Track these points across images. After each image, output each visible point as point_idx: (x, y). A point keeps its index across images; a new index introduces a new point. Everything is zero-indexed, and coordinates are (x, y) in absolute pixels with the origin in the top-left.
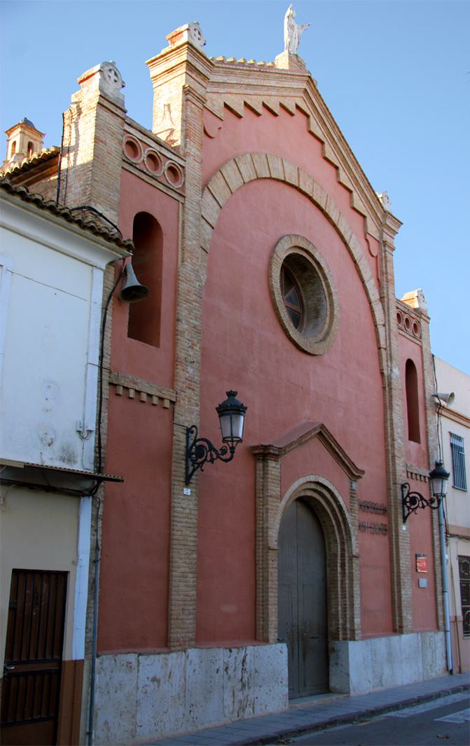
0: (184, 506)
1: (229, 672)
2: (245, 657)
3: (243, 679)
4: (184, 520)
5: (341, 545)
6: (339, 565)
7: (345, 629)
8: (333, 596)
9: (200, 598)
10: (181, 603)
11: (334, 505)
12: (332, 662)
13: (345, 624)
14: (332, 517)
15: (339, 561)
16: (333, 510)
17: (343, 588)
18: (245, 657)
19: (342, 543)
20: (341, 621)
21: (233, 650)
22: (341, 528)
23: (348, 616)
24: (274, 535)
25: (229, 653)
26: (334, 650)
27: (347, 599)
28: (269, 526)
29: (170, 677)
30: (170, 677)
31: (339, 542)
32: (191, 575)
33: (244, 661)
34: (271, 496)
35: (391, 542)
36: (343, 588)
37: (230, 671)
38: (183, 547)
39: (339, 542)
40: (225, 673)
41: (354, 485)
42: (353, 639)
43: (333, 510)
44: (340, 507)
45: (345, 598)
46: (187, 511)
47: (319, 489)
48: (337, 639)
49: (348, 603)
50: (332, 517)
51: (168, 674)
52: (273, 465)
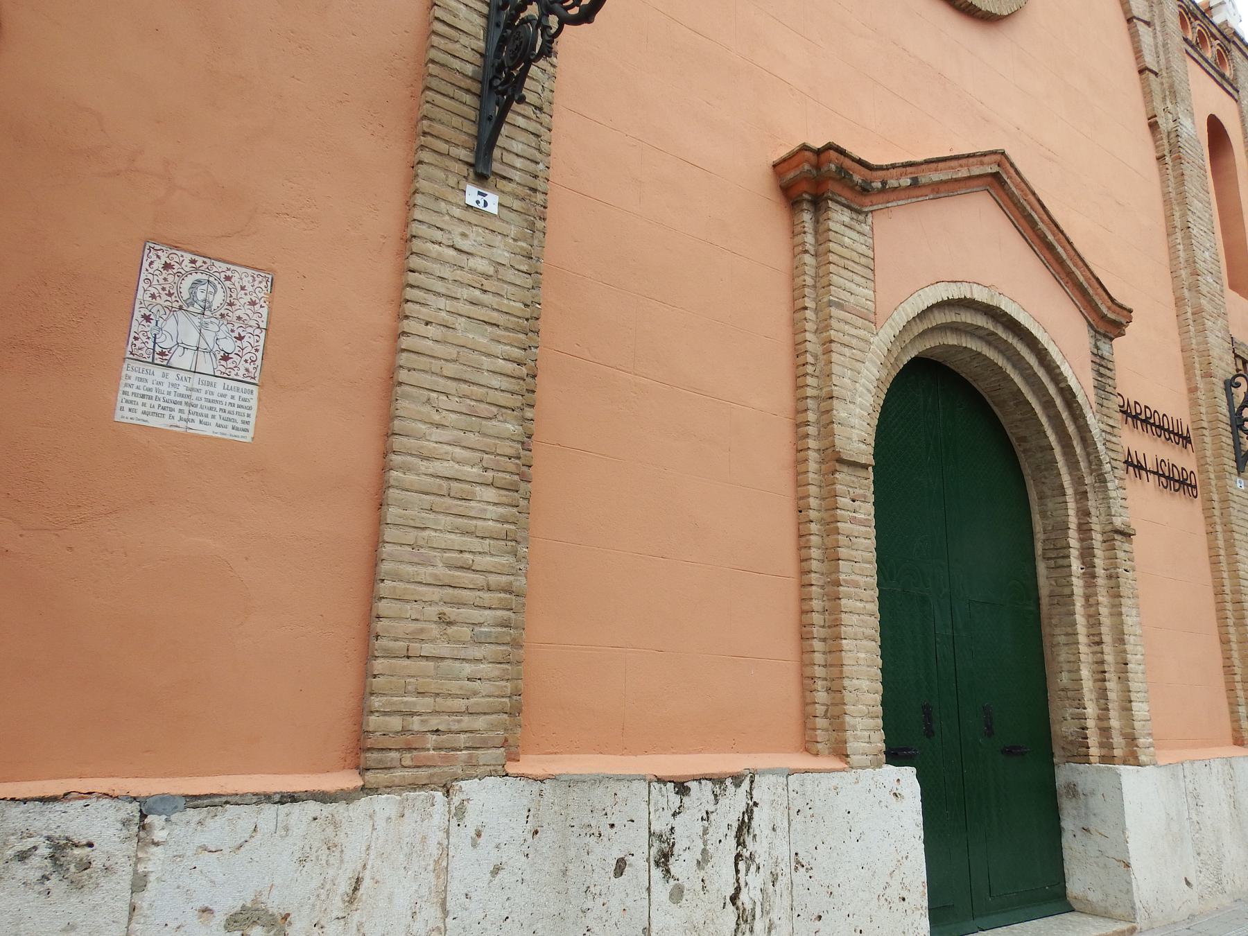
0: (465, 245)
1: (675, 868)
2: (749, 812)
3: (744, 897)
4: (465, 293)
5: (1077, 501)
6: (1074, 553)
7: (1105, 731)
8: (1063, 657)
9: (1068, 256)
10: (435, 594)
11: (1052, 390)
12: (1068, 824)
13: (1103, 717)
14: (1044, 420)
15: (1074, 542)
16: (1048, 404)
17: (1094, 620)
18: (749, 812)
19: (1082, 495)
20: (1091, 710)
21: (693, 785)
22: (1074, 454)
23: (1112, 695)
24: (855, 421)
25: (675, 800)
26: (1072, 790)
27: (1107, 648)
28: (836, 391)
29: (352, 898)
30: (352, 898)
31: (1069, 491)
32: (490, 494)
33: (744, 828)
34: (840, 306)
35: (1208, 516)
36: (1094, 620)
37: (681, 867)
38: (452, 386)
39: (1069, 491)
40: (657, 873)
41: (1105, 348)
42: (1132, 759)
43: (1048, 404)
44: (1068, 395)
45: (1100, 643)
46: (481, 265)
47: (967, 317)
48: (1085, 759)
49: (1109, 658)
50: (1044, 420)
51: (344, 887)
52: (846, 219)
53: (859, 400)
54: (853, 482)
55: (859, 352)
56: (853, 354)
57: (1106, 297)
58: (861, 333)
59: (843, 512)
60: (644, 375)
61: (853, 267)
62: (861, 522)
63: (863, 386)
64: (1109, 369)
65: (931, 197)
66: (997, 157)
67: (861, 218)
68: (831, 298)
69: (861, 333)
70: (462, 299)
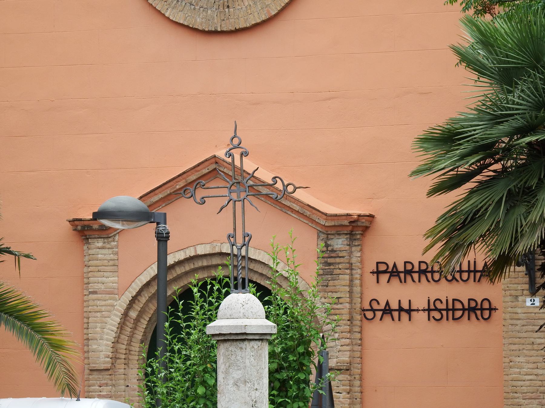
53: (105, 337)
54: (100, 378)
55: (107, 312)
56: (102, 315)
57: (320, 214)
58: (109, 302)
59: (93, 393)
60: (7, 348)
61: (104, 269)
62: (104, 396)
63: (109, 329)
64: (341, 257)
65: (163, 205)
66: (213, 160)
67: (110, 239)
68: (90, 290)
69: (109, 302)
70: (246, 197)
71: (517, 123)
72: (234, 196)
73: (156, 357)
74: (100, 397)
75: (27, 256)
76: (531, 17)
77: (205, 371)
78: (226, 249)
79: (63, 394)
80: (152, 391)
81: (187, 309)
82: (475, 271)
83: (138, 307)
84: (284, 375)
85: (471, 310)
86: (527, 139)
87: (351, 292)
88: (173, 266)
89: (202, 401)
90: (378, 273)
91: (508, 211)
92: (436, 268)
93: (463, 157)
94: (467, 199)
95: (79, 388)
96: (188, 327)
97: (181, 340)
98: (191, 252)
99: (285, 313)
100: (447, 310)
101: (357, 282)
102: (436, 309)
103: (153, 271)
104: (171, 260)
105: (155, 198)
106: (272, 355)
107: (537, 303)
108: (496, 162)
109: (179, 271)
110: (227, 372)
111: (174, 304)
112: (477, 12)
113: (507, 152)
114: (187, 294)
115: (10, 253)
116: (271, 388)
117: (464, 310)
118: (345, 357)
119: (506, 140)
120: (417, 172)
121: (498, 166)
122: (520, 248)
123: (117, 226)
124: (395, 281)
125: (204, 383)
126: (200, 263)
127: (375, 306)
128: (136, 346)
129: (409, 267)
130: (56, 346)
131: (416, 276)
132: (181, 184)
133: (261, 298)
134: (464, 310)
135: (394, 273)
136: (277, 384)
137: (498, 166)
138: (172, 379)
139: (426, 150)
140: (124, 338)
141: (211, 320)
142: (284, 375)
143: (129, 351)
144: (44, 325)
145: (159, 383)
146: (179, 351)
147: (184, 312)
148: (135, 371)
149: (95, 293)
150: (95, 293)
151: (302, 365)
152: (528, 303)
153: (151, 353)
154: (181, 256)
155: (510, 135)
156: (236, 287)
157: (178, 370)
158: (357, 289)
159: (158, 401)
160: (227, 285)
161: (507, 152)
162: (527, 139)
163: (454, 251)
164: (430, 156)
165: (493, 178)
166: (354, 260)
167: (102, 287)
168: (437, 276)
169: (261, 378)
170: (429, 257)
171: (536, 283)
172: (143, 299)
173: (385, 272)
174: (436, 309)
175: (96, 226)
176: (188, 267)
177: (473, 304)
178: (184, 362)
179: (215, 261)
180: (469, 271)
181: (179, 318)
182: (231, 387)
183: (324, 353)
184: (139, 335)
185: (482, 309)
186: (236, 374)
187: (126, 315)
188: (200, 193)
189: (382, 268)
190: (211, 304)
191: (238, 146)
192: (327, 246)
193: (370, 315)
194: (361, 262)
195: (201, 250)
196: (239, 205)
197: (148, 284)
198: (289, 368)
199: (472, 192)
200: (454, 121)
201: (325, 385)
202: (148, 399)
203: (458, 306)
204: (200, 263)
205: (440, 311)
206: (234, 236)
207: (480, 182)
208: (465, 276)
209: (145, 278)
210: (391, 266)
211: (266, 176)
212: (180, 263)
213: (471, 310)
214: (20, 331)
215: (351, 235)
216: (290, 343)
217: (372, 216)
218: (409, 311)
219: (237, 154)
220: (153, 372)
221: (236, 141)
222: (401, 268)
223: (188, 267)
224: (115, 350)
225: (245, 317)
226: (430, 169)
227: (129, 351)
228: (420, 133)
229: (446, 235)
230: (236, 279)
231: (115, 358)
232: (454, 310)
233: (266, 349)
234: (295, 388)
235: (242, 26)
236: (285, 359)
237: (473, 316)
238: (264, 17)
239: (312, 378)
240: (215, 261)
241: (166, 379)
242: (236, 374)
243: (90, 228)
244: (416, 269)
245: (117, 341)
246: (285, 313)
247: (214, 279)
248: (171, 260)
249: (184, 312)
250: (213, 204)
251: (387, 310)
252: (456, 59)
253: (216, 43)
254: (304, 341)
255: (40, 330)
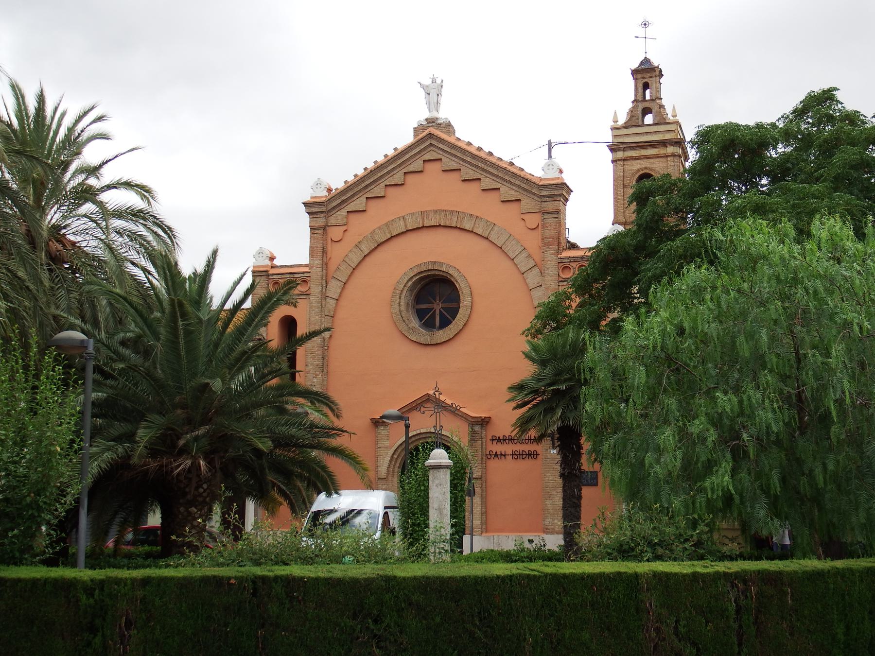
71: (548, 381)
72: (436, 411)
73: (405, 475)
74: (382, 489)
75: (354, 434)
76: (553, 340)
77: (424, 480)
78: (433, 430)
79: (367, 489)
80: (403, 489)
81: (417, 455)
82: (531, 439)
83: (397, 453)
84: (456, 482)
85: (530, 455)
86: (552, 388)
87: (482, 448)
88: (411, 437)
89: (423, 492)
90: (492, 440)
91: (544, 416)
92: (516, 438)
93: (526, 395)
94: (528, 411)
95: (374, 486)
96: (417, 462)
97: (415, 468)
98: (418, 432)
99: (456, 457)
100: (520, 455)
101: (484, 444)
102: (515, 455)
103: (404, 439)
104: (410, 435)
105: (404, 410)
106: (451, 474)
107: (555, 452)
108: (539, 397)
109: (414, 439)
110: (433, 481)
111: (411, 453)
112: (532, 338)
113: (544, 393)
114: (417, 449)
115: (347, 432)
116: (451, 487)
117: (526, 455)
118: (480, 474)
119: (543, 388)
120: (507, 401)
121: (540, 399)
122: (549, 431)
123: (390, 422)
124: (499, 443)
125: (424, 485)
126: (422, 436)
127: (491, 453)
128: (396, 469)
129: (505, 438)
130: (365, 470)
131: (507, 441)
132: (415, 405)
133: (446, 451)
134: (526, 455)
135: (499, 440)
136: (453, 485)
137: (540, 399)
138: (411, 483)
139: (512, 392)
140: (392, 466)
141: (427, 460)
142: (456, 482)
143: (393, 471)
144: (360, 461)
145: (406, 485)
146: (414, 472)
147: (416, 456)
148: (396, 479)
149: (380, 448)
150: (380, 448)
151: (463, 477)
152: (552, 452)
153: (403, 473)
154: (414, 433)
155: (545, 386)
156: (437, 447)
157: (413, 479)
158: (484, 446)
159: (405, 492)
160: (432, 446)
161: (544, 393)
162: (552, 388)
163: (523, 432)
164: (513, 394)
165: (538, 403)
166: (483, 435)
167: (383, 445)
168: (516, 441)
169: (447, 483)
170: (513, 434)
171: (767, 538)
172: (399, 450)
173: (495, 440)
174: (515, 455)
175: (381, 421)
176: (417, 438)
177: (530, 453)
178: (416, 477)
179: (428, 435)
180: (528, 440)
181: (414, 459)
182: (435, 487)
183: (471, 473)
184: (398, 465)
185: (533, 455)
186: (437, 482)
187: (392, 456)
188: (423, 409)
189: (494, 438)
190: (426, 453)
191: (437, 391)
192: (472, 429)
193: (489, 457)
194: (486, 436)
195: (422, 431)
196: (438, 414)
197: (401, 444)
198: (457, 479)
199: (530, 409)
200: (523, 380)
201: (472, 486)
202: (401, 491)
203: (524, 453)
204: (422, 436)
205: (517, 455)
206: (436, 427)
207: (533, 405)
208: (527, 441)
209: (400, 442)
210: (498, 437)
211: (449, 402)
212: (414, 436)
213: (530, 455)
214: (351, 464)
215: (482, 425)
216: (458, 469)
217: (490, 417)
218: (505, 455)
219: (437, 394)
220: (403, 480)
221: (437, 389)
222: (501, 438)
223: (417, 438)
224: (388, 471)
225: (440, 459)
226: (513, 400)
227: (393, 471)
228: (510, 386)
229: (519, 426)
230: (437, 442)
231: (388, 474)
232: (522, 455)
233: (449, 471)
234: (460, 487)
235: (439, 342)
236: (456, 475)
237: (530, 457)
238: (447, 339)
239: (467, 484)
240: (428, 435)
241: (408, 483)
242: (437, 482)
243: (378, 422)
244: (508, 438)
245: (389, 467)
246: (456, 457)
247: (427, 443)
248: (410, 435)
249: (416, 456)
250: (428, 414)
251: (496, 455)
252: (524, 356)
253: (429, 349)
254: (464, 468)
255: (358, 463)
